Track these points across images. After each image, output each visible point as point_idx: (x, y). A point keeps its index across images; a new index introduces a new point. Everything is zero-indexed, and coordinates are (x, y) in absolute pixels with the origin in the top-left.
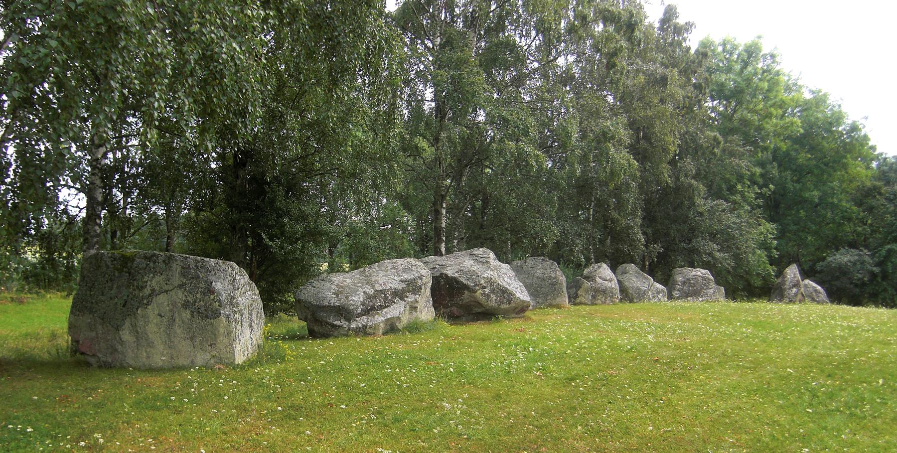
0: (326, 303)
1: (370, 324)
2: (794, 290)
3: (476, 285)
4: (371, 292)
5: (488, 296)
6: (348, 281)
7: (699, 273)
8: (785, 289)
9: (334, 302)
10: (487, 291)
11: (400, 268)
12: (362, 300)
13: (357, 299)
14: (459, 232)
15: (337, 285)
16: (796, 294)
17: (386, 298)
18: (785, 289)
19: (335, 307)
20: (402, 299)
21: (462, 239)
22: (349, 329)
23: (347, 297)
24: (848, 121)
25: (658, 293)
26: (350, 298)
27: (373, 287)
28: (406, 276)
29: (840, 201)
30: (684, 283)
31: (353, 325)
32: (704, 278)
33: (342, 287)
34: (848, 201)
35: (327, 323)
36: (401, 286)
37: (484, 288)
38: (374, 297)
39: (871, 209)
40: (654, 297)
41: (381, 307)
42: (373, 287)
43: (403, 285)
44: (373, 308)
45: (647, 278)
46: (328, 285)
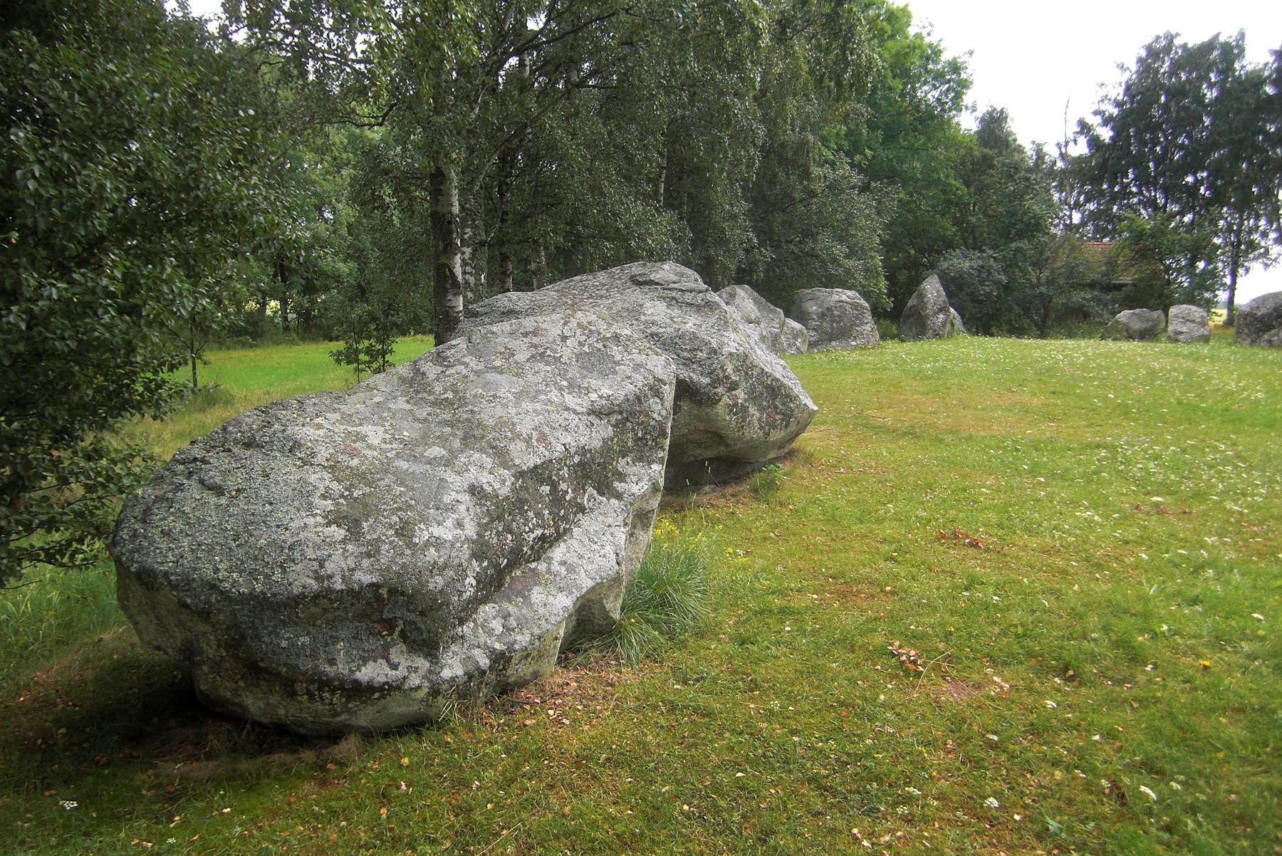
0: (301, 580)
1: (522, 639)
2: (941, 316)
3: (716, 382)
4: (500, 483)
5: (744, 409)
6: (375, 435)
7: (844, 298)
8: (927, 317)
9: (347, 565)
10: (741, 394)
11: (566, 353)
12: (471, 530)
13: (450, 532)
14: (474, 227)
15: (333, 467)
16: (944, 324)
17: (557, 500)
18: (927, 317)
19: (353, 594)
20: (605, 488)
21: (482, 244)
22: (435, 692)
23: (404, 531)
24: (946, 57)
25: (795, 337)
26: (421, 536)
27: (502, 457)
28: (606, 389)
29: (947, 177)
30: (822, 316)
31: (452, 668)
32: (856, 306)
33: (361, 476)
34: (956, 179)
35: (325, 683)
36: (596, 435)
37: (733, 386)
38: (518, 504)
39: (981, 190)
40: (789, 345)
41: (545, 543)
42: (502, 457)
43: (604, 430)
44: (517, 558)
45: (775, 312)
46: (286, 471)
